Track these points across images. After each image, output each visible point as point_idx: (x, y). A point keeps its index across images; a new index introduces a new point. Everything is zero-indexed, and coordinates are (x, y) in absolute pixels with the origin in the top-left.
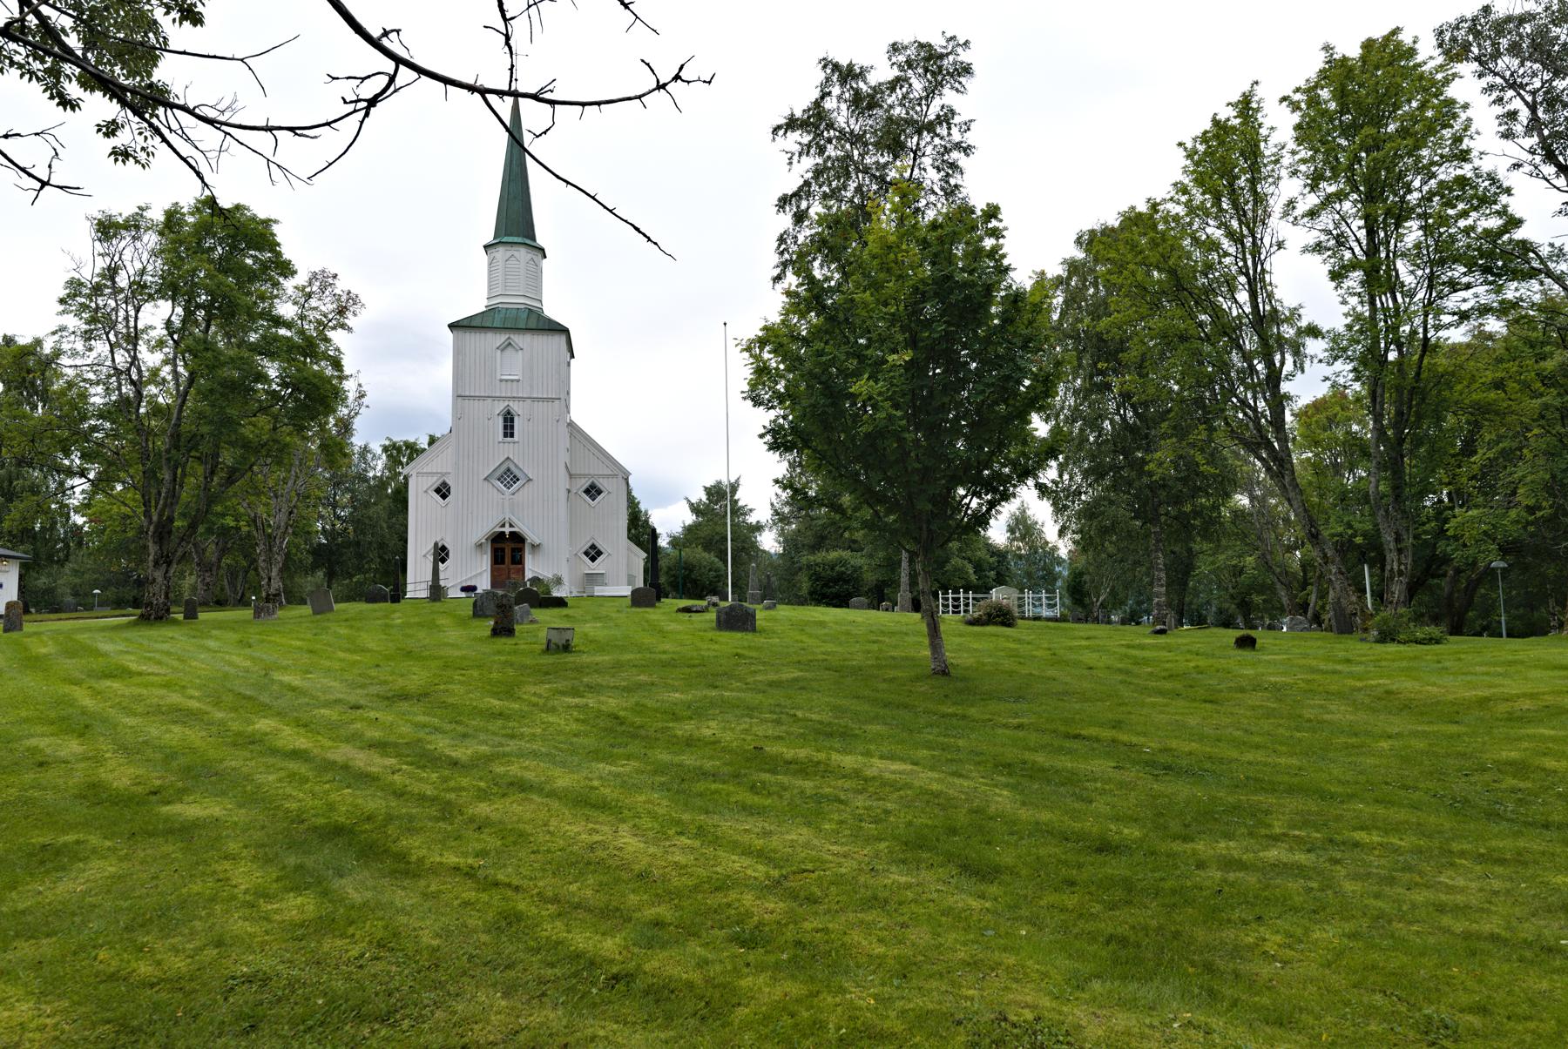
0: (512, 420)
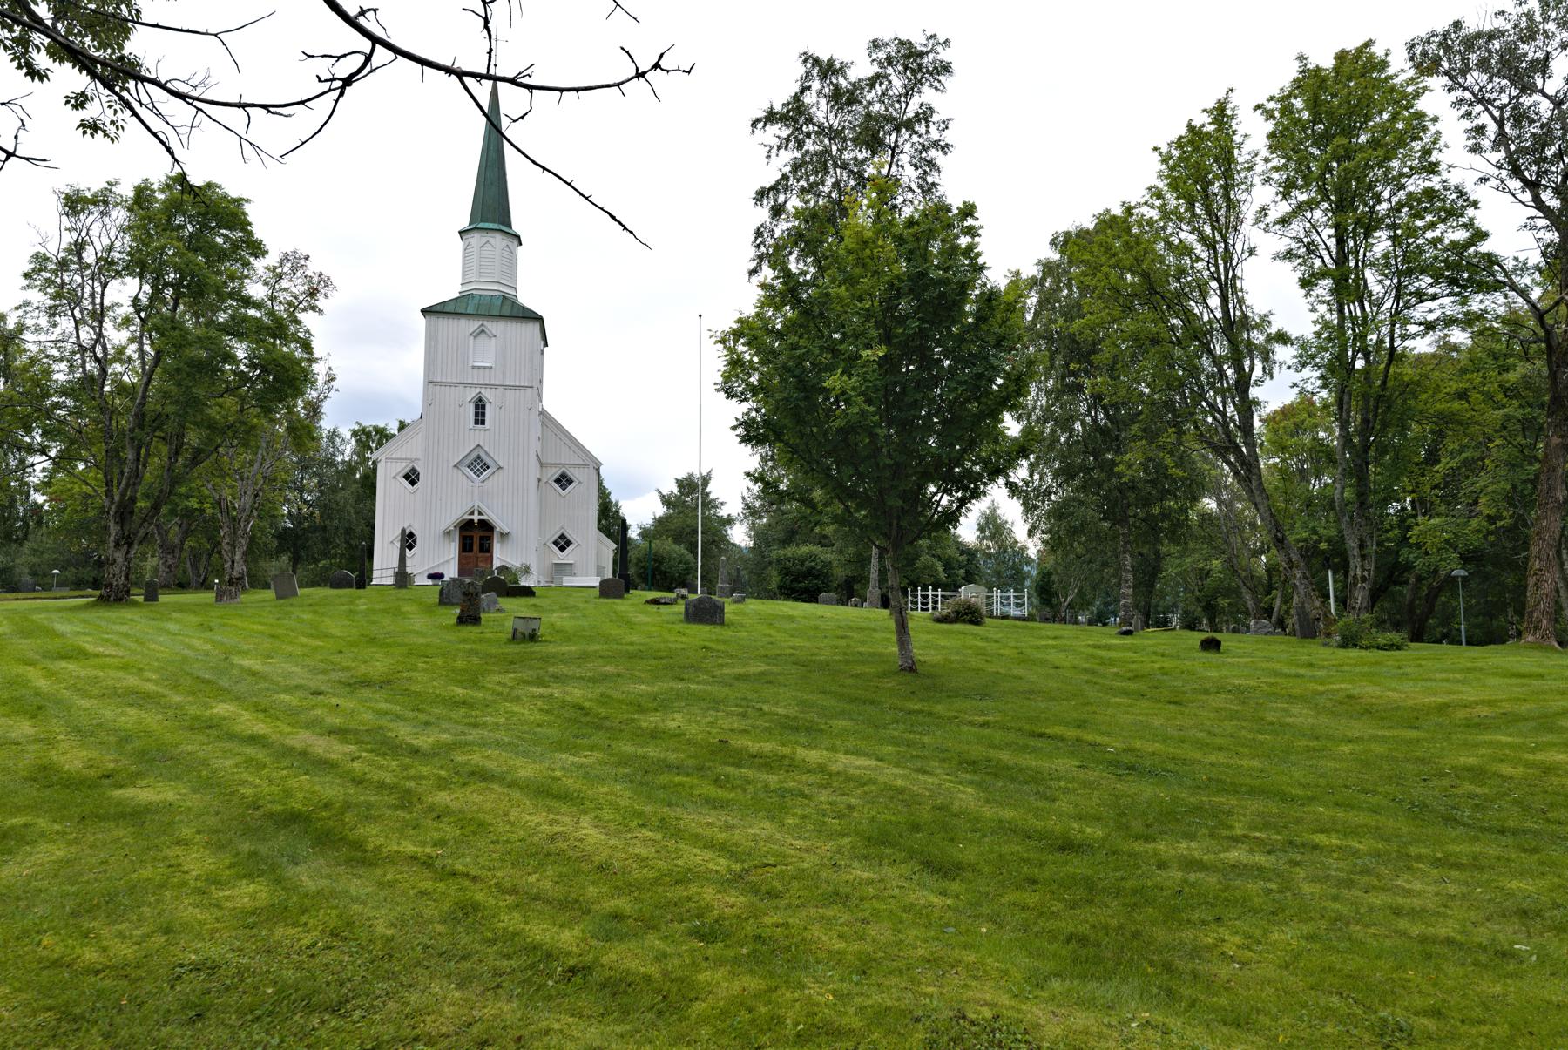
0: (484, 407)
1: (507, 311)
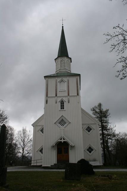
0: (63, 103)
1: (69, 74)
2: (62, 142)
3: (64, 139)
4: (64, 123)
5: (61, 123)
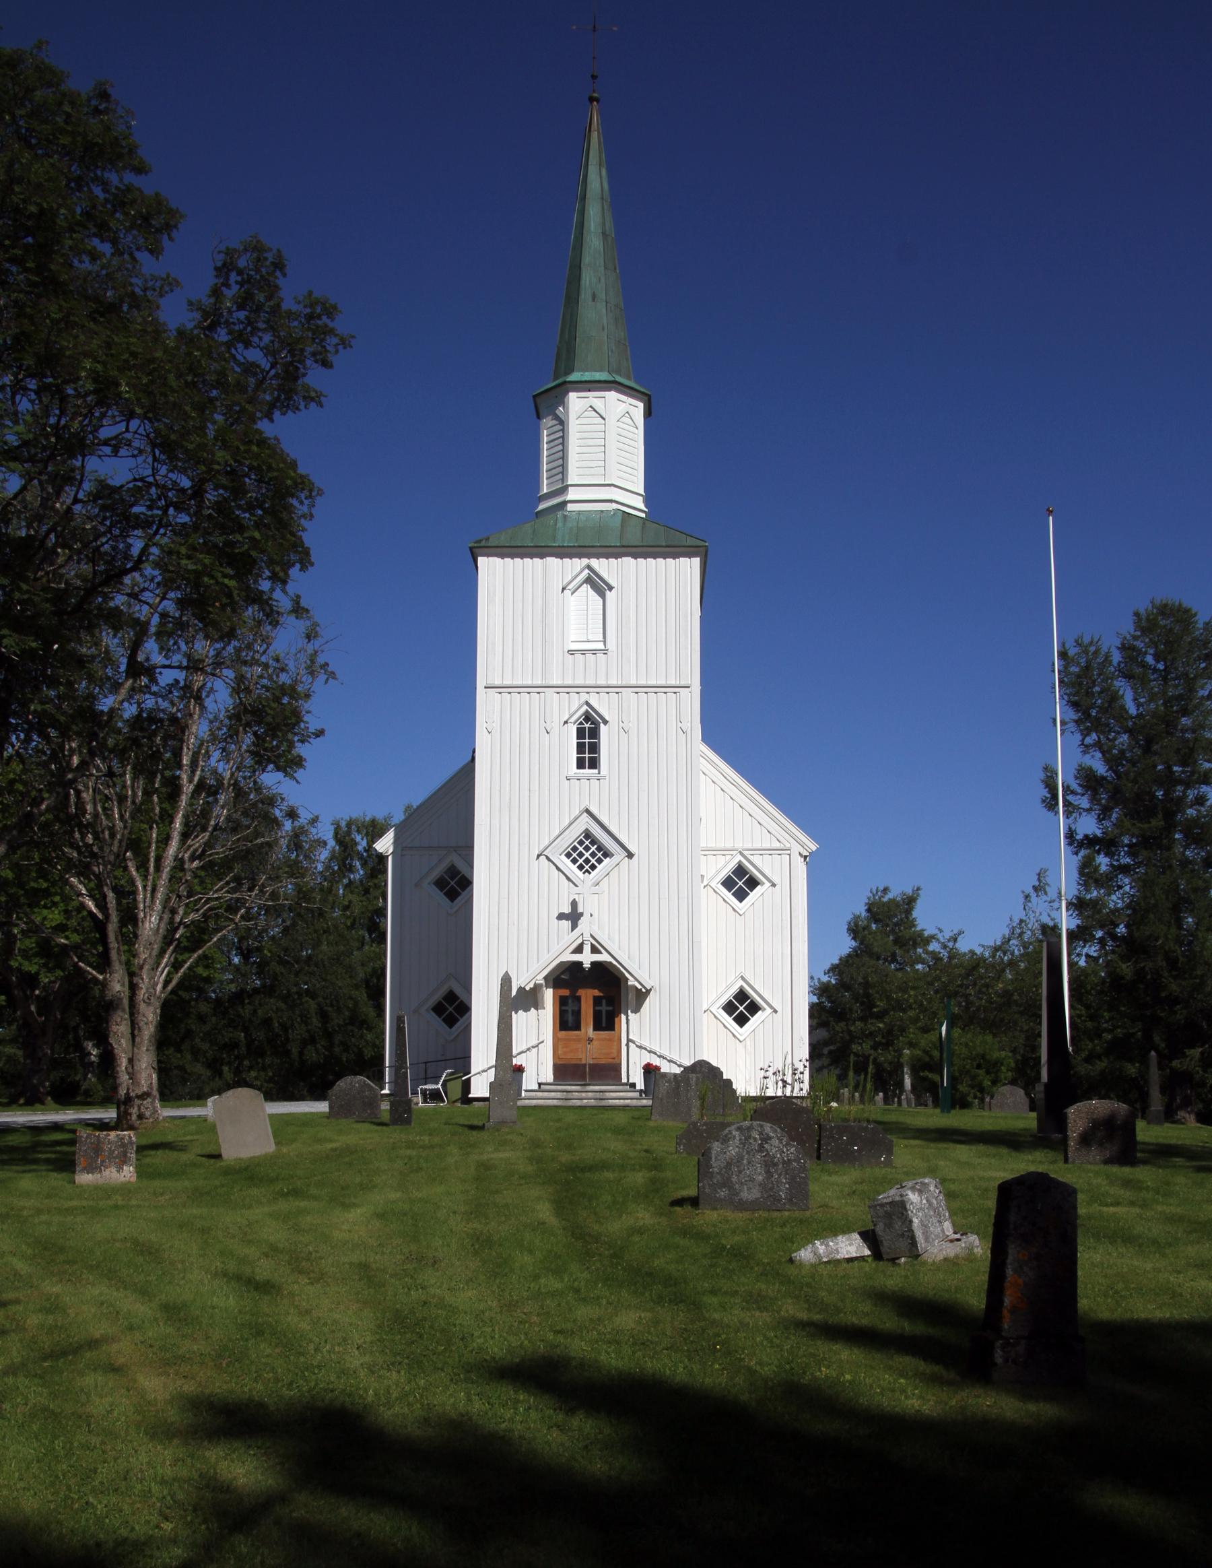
0: (594, 733)
2: (587, 965)
3: (594, 950)
4: (593, 855)
5: (581, 855)
